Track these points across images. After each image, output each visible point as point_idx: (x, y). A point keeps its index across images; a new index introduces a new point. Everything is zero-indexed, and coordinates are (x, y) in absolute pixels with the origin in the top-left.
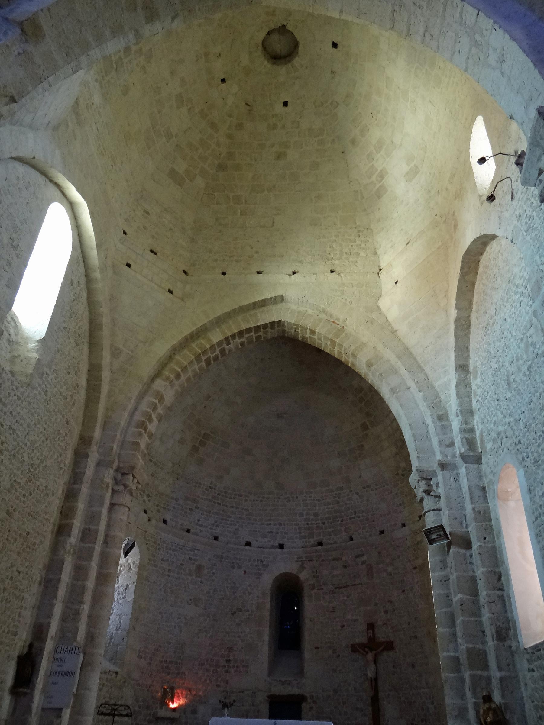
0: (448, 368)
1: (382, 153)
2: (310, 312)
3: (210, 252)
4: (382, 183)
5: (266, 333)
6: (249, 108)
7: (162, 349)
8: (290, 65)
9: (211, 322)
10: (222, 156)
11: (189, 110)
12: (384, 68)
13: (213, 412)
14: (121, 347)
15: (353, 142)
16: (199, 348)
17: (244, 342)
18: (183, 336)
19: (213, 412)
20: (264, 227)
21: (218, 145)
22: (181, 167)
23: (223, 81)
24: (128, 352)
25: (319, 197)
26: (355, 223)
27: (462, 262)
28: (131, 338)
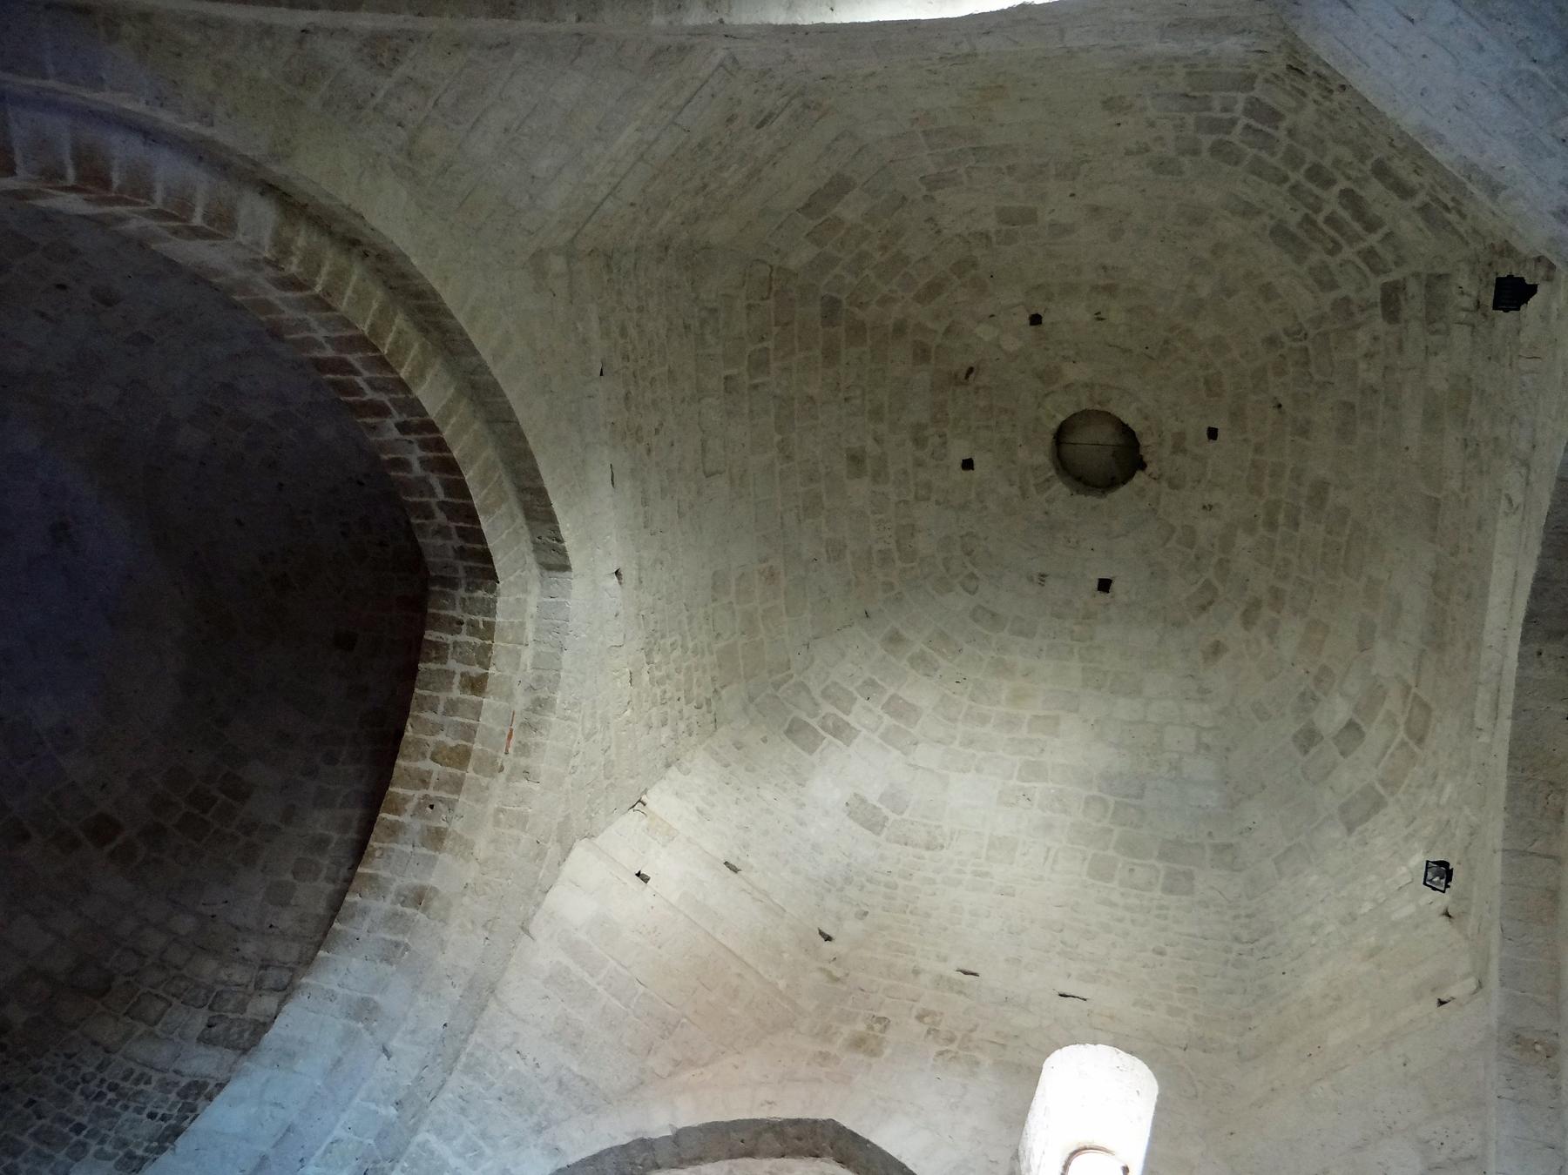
0: (488, 1151)
1: (888, 720)
2: (527, 656)
3: (640, 309)
4: (822, 732)
5: (442, 532)
6: (962, 376)
7: (390, 215)
8: (1052, 472)
9: (482, 368)
10: (857, 310)
11: (985, 236)
12: (1076, 711)
13: (43, 315)
14: (401, 71)
15: (895, 639)
16: (395, 342)
17: (410, 471)
18: (437, 286)
19: (43, 315)
20: (704, 450)
21: (885, 301)
22: (850, 210)
23: (1036, 320)
24: (381, 94)
25: (772, 576)
26: (723, 687)
27: (815, 1121)
28: (431, 103)
